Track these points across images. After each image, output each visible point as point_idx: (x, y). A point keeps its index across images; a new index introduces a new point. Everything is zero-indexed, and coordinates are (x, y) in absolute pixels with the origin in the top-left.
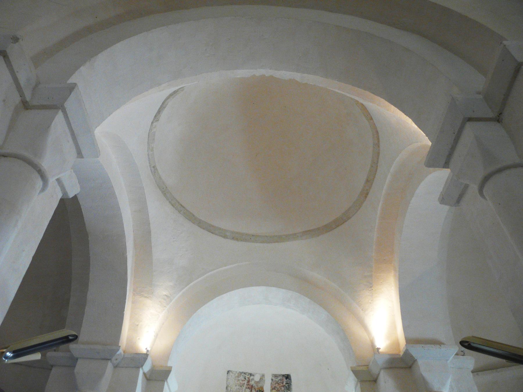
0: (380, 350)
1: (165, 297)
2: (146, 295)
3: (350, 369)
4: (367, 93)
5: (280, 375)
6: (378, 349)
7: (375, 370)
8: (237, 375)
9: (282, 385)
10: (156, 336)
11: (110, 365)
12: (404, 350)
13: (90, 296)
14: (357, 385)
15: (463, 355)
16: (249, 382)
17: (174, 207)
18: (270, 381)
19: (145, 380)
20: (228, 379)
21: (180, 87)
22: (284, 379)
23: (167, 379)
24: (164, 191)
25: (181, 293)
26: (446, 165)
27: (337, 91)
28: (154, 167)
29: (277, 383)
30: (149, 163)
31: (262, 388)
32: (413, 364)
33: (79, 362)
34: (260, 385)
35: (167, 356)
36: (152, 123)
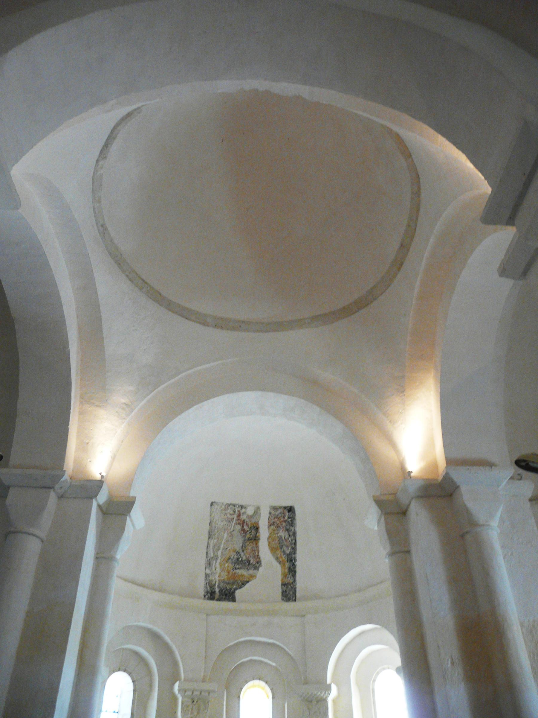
0: (412, 475)
1: (124, 406)
2: (97, 403)
3: (372, 499)
4: (406, 117)
5: (280, 508)
6: (410, 473)
7: (404, 500)
8: (223, 507)
9: (283, 519)
10: (114, 458)
11: (53, 497)
12: (444, 474)
13: (22, 404)
14: (379, 521)
15: (521, 479)
16: (239, 516)
17: (132, 282)
18: (267, 515)
19: (100, 513)
20: (211, 513)
21: (134, 107)
22: (286, 511)
23: (129, 512)
24: (119, 260)
25: (145, 401)
26: (510, 221)
27: (361, 113)
28: (102, 226)
29: (277, 517)
30: (96, 220)
31: (257, 523)
32: (454, 491)
33: (12, 492)
34: (253, 520)
35: (129, 482)
36: (97, 161)
